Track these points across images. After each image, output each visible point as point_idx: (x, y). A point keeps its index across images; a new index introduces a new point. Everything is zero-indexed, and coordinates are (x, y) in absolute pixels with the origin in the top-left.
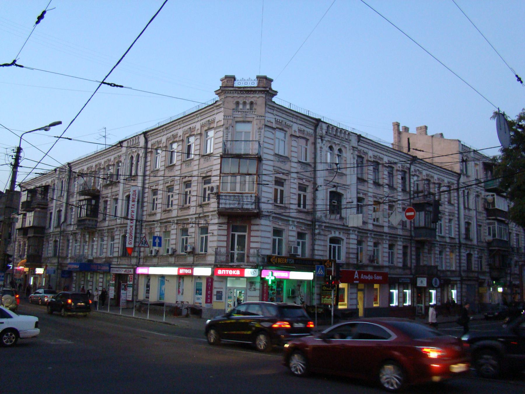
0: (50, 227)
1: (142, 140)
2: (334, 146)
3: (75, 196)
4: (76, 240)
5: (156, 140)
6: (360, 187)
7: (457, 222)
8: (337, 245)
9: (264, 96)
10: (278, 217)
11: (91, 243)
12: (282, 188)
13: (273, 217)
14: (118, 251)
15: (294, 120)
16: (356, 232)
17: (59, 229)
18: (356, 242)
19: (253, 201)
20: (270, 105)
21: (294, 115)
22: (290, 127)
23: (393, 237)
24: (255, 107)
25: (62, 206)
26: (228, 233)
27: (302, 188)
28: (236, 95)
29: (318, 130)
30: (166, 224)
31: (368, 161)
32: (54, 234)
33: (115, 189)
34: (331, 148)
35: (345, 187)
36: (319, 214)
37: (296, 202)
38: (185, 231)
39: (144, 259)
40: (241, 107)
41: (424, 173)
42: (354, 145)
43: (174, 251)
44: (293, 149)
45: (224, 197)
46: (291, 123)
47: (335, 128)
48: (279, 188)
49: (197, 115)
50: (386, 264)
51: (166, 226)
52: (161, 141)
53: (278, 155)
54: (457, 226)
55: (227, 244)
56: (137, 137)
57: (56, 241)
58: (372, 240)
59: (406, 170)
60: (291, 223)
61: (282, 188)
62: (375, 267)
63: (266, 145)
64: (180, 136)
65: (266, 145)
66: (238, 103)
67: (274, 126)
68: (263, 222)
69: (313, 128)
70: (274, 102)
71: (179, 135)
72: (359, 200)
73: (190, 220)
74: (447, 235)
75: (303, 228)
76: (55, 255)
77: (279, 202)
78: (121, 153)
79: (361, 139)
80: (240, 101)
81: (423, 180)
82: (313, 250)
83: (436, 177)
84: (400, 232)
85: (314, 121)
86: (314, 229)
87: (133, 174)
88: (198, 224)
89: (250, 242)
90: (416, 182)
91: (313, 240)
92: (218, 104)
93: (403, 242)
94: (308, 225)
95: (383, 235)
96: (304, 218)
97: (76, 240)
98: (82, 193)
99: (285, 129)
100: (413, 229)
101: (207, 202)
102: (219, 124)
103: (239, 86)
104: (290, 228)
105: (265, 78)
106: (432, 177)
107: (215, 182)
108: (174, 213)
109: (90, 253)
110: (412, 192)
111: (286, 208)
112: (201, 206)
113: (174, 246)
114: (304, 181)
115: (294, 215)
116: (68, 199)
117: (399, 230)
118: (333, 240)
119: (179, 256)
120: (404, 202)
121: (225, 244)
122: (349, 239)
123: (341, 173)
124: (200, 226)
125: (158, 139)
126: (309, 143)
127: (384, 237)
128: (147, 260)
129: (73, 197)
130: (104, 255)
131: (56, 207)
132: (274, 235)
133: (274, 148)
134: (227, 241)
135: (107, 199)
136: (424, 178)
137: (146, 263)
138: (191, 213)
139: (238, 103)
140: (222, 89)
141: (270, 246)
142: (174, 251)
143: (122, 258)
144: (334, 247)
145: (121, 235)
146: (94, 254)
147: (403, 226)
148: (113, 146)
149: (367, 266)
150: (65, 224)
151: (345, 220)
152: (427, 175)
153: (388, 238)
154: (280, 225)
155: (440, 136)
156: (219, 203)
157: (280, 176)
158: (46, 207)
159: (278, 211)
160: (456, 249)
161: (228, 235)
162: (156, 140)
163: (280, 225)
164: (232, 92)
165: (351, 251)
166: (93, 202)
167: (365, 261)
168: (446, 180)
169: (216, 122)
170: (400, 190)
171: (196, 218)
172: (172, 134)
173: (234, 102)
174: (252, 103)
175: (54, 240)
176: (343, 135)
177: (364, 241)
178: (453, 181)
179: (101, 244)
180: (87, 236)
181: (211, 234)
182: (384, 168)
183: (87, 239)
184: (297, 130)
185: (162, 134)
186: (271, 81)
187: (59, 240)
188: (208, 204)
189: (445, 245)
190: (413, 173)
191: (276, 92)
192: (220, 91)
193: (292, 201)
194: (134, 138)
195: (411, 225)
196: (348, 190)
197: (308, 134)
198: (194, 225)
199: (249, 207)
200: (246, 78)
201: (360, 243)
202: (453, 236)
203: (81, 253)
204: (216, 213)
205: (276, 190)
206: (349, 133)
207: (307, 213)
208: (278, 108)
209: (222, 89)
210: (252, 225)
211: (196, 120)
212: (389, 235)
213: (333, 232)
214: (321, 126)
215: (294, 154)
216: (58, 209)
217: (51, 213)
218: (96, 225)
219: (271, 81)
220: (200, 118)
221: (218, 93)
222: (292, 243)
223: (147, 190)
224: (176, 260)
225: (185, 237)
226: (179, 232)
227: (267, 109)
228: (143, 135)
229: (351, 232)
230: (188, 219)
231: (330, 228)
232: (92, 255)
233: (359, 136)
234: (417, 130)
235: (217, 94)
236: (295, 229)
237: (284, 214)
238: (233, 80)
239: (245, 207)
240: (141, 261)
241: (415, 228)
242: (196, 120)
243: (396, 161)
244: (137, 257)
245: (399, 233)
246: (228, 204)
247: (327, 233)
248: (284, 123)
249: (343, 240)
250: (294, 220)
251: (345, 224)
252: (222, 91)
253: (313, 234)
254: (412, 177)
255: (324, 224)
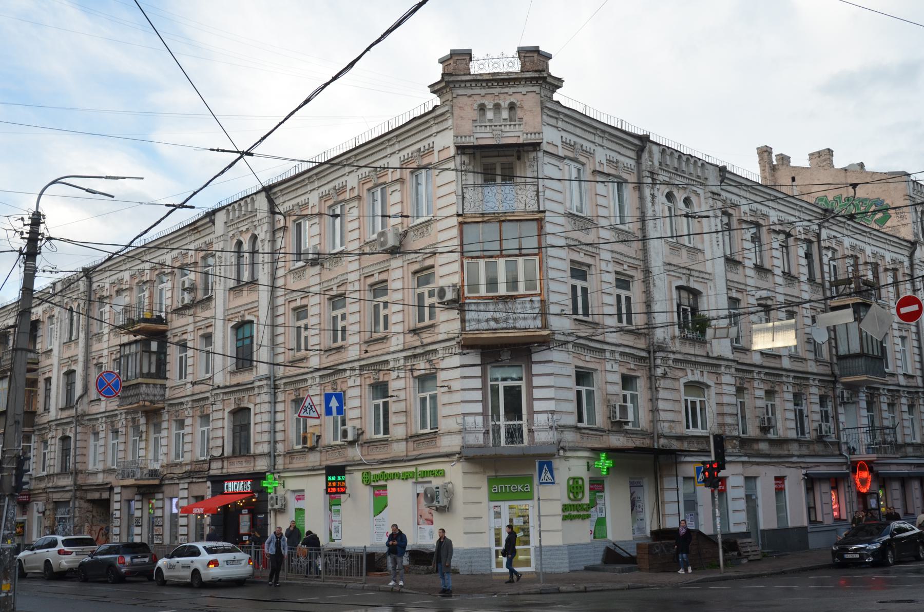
0: (47, 410)
1: (262, 203)
2: (675, 193)
3: (105, 338)
4: (116, 432)
5: (295, 202)
6: (731, 276)
7: (915, 344)
8: (697, 400)
9: (537, 89)
10: (581, 345)
11: (152, 436)
12: (584, 284)
13: (576, 345)
14: (223, 446)
15: (598, 140)
16: (733, 370)
17: (72, 412)
18: (733, 390)
19: (537, 311)
20: (550, 109)
21: (596, 129)
22: (590, 154)
23: (802, 378)
24: (519, 113)
25: (76, 361)
26: (484, 383)
27: (623, 282)
28: (477, 91)
29: (645, 155)
30: (334, 378)
31: (741, 221)
32: (60, 423)
33: (202, 314)
34: (670, 196)
35: (706, 277)
36: (660, 334)
37: (614, 310)
38: (381, 389)
39: (284, 455)
40: (490, 115)
41: (847, 242)
42: (715, 189)
43: (360, 433)
44: (601, 201)
45: (473, 307)
46: (593, 147)
47: (676, 155)
48: (579, 284)
49: (389, 140)
50: (792, 434)
51: (335, 382)
52: (344, 187)
53: (570, 214)
54: (916, 351)
55: (485, 407)
56: (249, 200)
57: (65, 439)
58: (762, 386)
59: (813, 239)
60: (608, 354)
61: (584, 284)
62: (772, 442)
63: (549, 194)
64: (353, 189)
65: (549, 194)
66: (482, 108)
67: (561, 153)
68: (556, 355)
69: (632, 154)
70: (558, 102)
71: (349, 187)
72: (734, 302)
73: (392, 365)
74: (900, 371)
75: (632, 366)
76: (64, 471)
77: (580, 311)
78: (212, 236)
79: (727, 175)
80: (486, 103)
81: (845, 257)
82: (655, 411)
83: (869, 250)
84: (812, 367)
85: (636, 142)
86: (651, 368)
87: (246, 277)
88: (412, 370)
89: (531, 399)
90: (832, 263)
91: (653, 389)
92: (438, 112)
93: (819, 387)
94: (641, 359)
95: (781, 375)
96: (631, 344)
97: (116, 432)
98: (127, 327)
99: (582, 159)
100: (835, 360)
101: (427, 322)
102: (445, 155)
103: (482, 72)
104: (608, 367)
105: (536, 50)
106: (862, 251)
107: (448, 273)
108: (353, 353)
109: (151, 456)
110: (827, 285)
111: (595, 325)
112: (415, 331)
113: (357, 424)
114: (626, 267)
115: (613, 338)
116: (88, 346)
117: (810, 363)
118: (695, 387)
119: (370, 443)
120: (816, 305)
121: (479, 408)
122: (720, 384)
123: (694, 248)
124: (416, 373)
125: (301, 200)
126: (628, 190)
127: (784, 379)
128: (292, 458)
129: (100, 340)
130: (187, 458)
131: (60, 364)
132: (578, 383)
133: (565, 199)
134: (484, 401)
135: (184, 337)
136: (846, 252)
137: (291, 466)
138: (392, 349)
139: (482, 108)
140: (447, 78)
141: (573, 407)
142: (360, 433)
143: (234, 460)
144: (693, 403)
145: (227, 410)
146: (161, 457)
147: (816, 355)
148: (321, 164)
149: (757, 440)
150: (85, 400)
151: (708, 345)
152: (853, 247)
153: (791, 380)
154: (588, 361)
155: (858, 168)
156: (463, 321)
157: (580, 257)
158: (35, 367)
159: (585, 331)
160: (919, 398)
161: (483, 389)
162: (295, 202)
163: (588, 361)
164: (468, 85)
165: (727, 410)
166: (154, 346)
167: (753, 431)
168: (888, 256)
169: (436, 153)
170: (804, 278)
171: (406, 358)
172: (331, 185)
173: (475, 106)
174: (512, 107)
175: (60, 436)
176: (692, 169)
177: (746, 389)
178: (900, 257)
179: (178, 435)
180: (142, 421)
181: (446, 389)
182: (773, 236)
183: (143, 428)
184: (604, 161)
185: (309, 188)
186: (548, 57)
187: (72, 435)
188: (385, 338)
189: (898, 391)
190: (827, 244)
191: (560, 80)
192: (443, 84)
193: (607, 310)
194: (242, 203)
195: (830, 351)
196: (710, 283)
197: (627, 169)
198: (402, 374)
199: (531, 323)
200: (495, 56)
201: (740, 390)
202: (910, 372)
203: (130, 458)
204: (453, 343)
205: (574, 288)
206: (703, 164)
207: (635, 333)
208: (566, 115)
209: (447, 78)
210: (533, 363)
211: (389, 151)
212: (792, 374)
213: (689, 371)
214: (650, 152)
215: (602, 212)
216: (65, 369)
217: (48, 380)
218: (164, 395)
219: (548, 57)
220: (397, 147)
221: (436, 89)
222: (614, 398)
223: (281, 310)
224: (324, 459)
225: (380, 402)
226: (368, 392)
227: (544, 117)
228: (263, 194)
229: (723, 369)
230: (387, 362)
231: (686, 362)
232: (156, 459)
233: (723, 170)
234: (810, 159)
235: (434, 92)
236: (616, 367)
237: (594, 338)
238: (468, 58)
239: (521, 324)
240: (280, 462)
241: (840, 358)
242: (389, 151)
243: (792, 219)
244: (269, 454)
245: (810, 370)
246: (482, 321)
247: (679, 374)
248: (578, 146)
249: (708, 387)
250: (613, 348)
251: (710, 354)
252: (448, 83)
253: (651, 378)
254: (824, 252)
255: (671, 356)
